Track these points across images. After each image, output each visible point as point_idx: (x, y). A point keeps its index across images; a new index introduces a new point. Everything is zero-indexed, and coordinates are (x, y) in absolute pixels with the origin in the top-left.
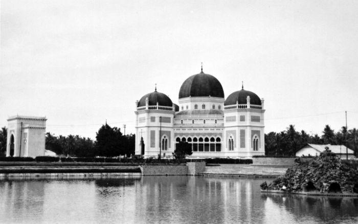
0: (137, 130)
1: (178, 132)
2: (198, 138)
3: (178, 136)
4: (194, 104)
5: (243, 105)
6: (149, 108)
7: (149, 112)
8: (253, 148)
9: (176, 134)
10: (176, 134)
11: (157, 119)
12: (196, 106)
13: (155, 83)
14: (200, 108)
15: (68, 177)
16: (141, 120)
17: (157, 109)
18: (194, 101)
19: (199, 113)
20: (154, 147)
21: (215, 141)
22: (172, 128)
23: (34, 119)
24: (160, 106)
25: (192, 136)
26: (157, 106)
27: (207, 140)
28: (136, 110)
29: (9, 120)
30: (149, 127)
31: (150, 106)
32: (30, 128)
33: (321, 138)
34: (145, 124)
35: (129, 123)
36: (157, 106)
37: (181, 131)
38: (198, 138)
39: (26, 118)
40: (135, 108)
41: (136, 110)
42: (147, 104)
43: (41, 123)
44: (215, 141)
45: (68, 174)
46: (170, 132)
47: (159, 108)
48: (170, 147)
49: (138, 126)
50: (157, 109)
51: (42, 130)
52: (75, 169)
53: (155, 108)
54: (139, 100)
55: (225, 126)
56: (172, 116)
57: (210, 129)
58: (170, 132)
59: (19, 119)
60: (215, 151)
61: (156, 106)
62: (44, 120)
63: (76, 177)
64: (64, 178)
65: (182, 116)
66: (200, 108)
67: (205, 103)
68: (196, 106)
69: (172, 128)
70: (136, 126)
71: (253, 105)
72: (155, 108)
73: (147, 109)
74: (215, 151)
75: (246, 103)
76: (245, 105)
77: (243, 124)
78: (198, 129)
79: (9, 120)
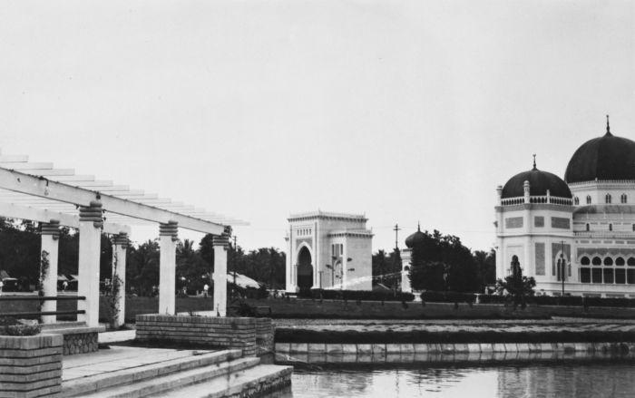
0: (502, 242)
1: (586, 246)
2: (614, 259)
3: (585, 255)
4: (605, 193)
5: (541, 197)
6: (531, 200)
7: (531, 208)
8: (556, 277)
9: (580, 251)
10: (580, 251)
11: (548, 222)
12: (608, 198)
13: (533, 153)
14: (616, 201)
15: (423, 358)
16: (516, 223)
17: (548, 202)
18: (606, 188)
19: (618, 210)
20: (543, 274)
21: (591, 264)
22: (573, 238)
23: (347, 219)
24: (552, 197)
25: (602, 254)
26: (548, 196)
27: (608, 261)
28: (499, 205)
29: (290, 220)
30: (531, 236)
31: (533, 197)
32: (350, 235)
33: (387, 256)
34: (524, 230)
35: (478, 229)
36: (548, 196)
37: (591, 245)
38: (614, 259)
39: (349, 217)
40: (496, 200)
41: (499, 205)
42: (527, 194)
43: (357, 225)
44: (591, 264)
45: (352, 348)
46: (569, 246)
47: (552, 201)
48: (570, 275)
49: (504, 235)
50: (548, 202)
51: (367, 240)
52: (440, 329)
53: (544, 201)
54: (503, 185)
55: (527, 239)
56: (569, 215)
57: (602, 241)
58: (569, 246)
59: (323, 218)
60: (626, 283)
61: (545, 197)
62: (363, 220)
63: (472, 357)
64: (498, 357)
65: (587, 216)
66: (616, 201)
67: (627, 193)
68: (608, 198)
69: (573, 238)
70: (500, 235)
71: (554, 198)
72: (544, 201)
73: (527, 201)
74: (626, 283)
75: (523, 195)
76: (522, 198)
77: (539, 231)
78: (626, 242)
79: (290, 220)
